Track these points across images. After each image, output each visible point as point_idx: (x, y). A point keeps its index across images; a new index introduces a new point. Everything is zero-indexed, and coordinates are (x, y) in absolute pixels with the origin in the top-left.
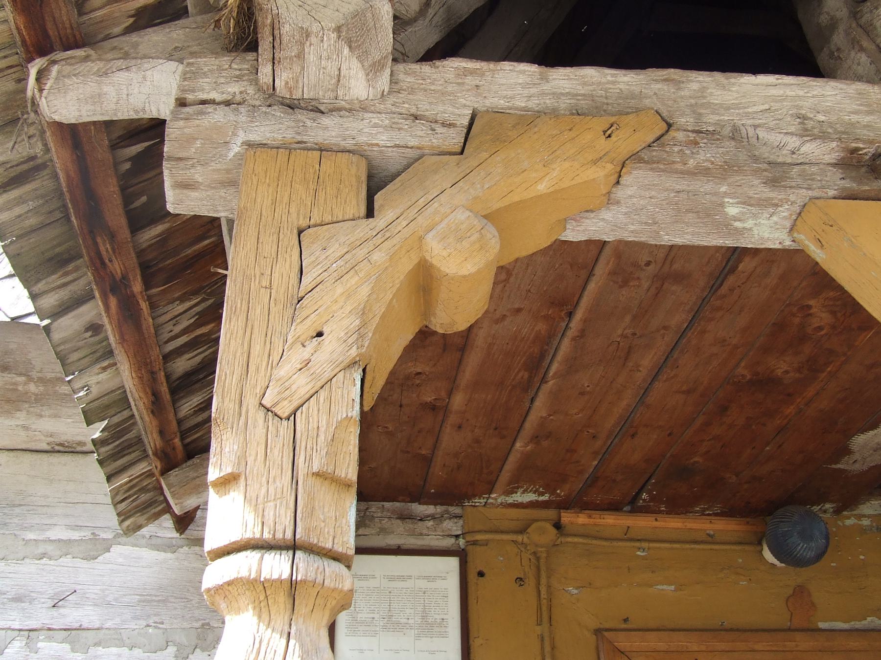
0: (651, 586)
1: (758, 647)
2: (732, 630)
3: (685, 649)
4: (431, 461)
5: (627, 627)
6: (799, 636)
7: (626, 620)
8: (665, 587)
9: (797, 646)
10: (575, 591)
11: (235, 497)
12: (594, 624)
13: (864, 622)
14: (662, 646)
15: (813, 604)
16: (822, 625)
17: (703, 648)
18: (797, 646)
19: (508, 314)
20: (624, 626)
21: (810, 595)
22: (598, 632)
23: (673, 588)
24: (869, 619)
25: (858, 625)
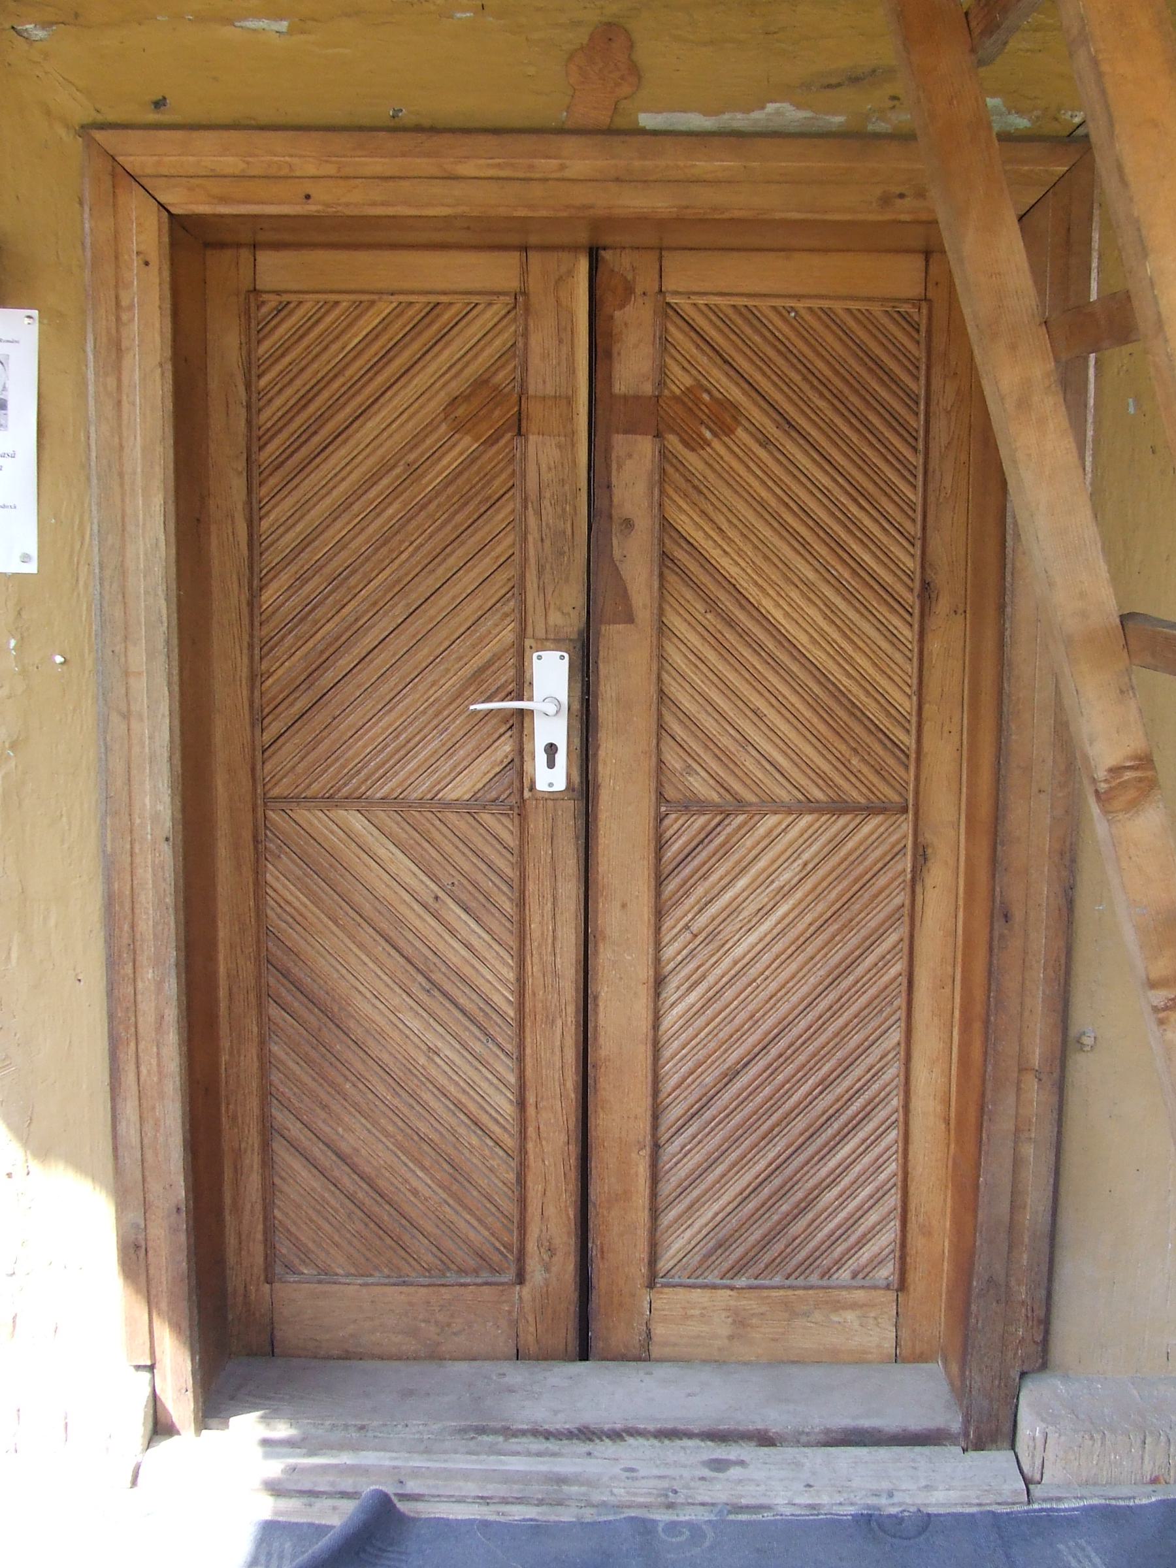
0: (229, 21)
1: (467, 169)
2: (418, 129)
3: (285, 172)
4: (648, 1359)
5: (161, 117)
6: (571, 144)
7: (159, 104)
8: (263, 24)
9: (562, 167)
10: (40, 34)
11: (1146, 825)
12: (82, 112)
13: (756, 115)
14: (231, 163)
15: (634, 70)
16: (647, 120)
17: (330, 169)
18: (562, 167)
19: (139, 1458)
20: (152, 117)
21: (631, 46)
22: (85, 129)
23: (283, 26)
24: (771, 107)
25: (738, 120)
